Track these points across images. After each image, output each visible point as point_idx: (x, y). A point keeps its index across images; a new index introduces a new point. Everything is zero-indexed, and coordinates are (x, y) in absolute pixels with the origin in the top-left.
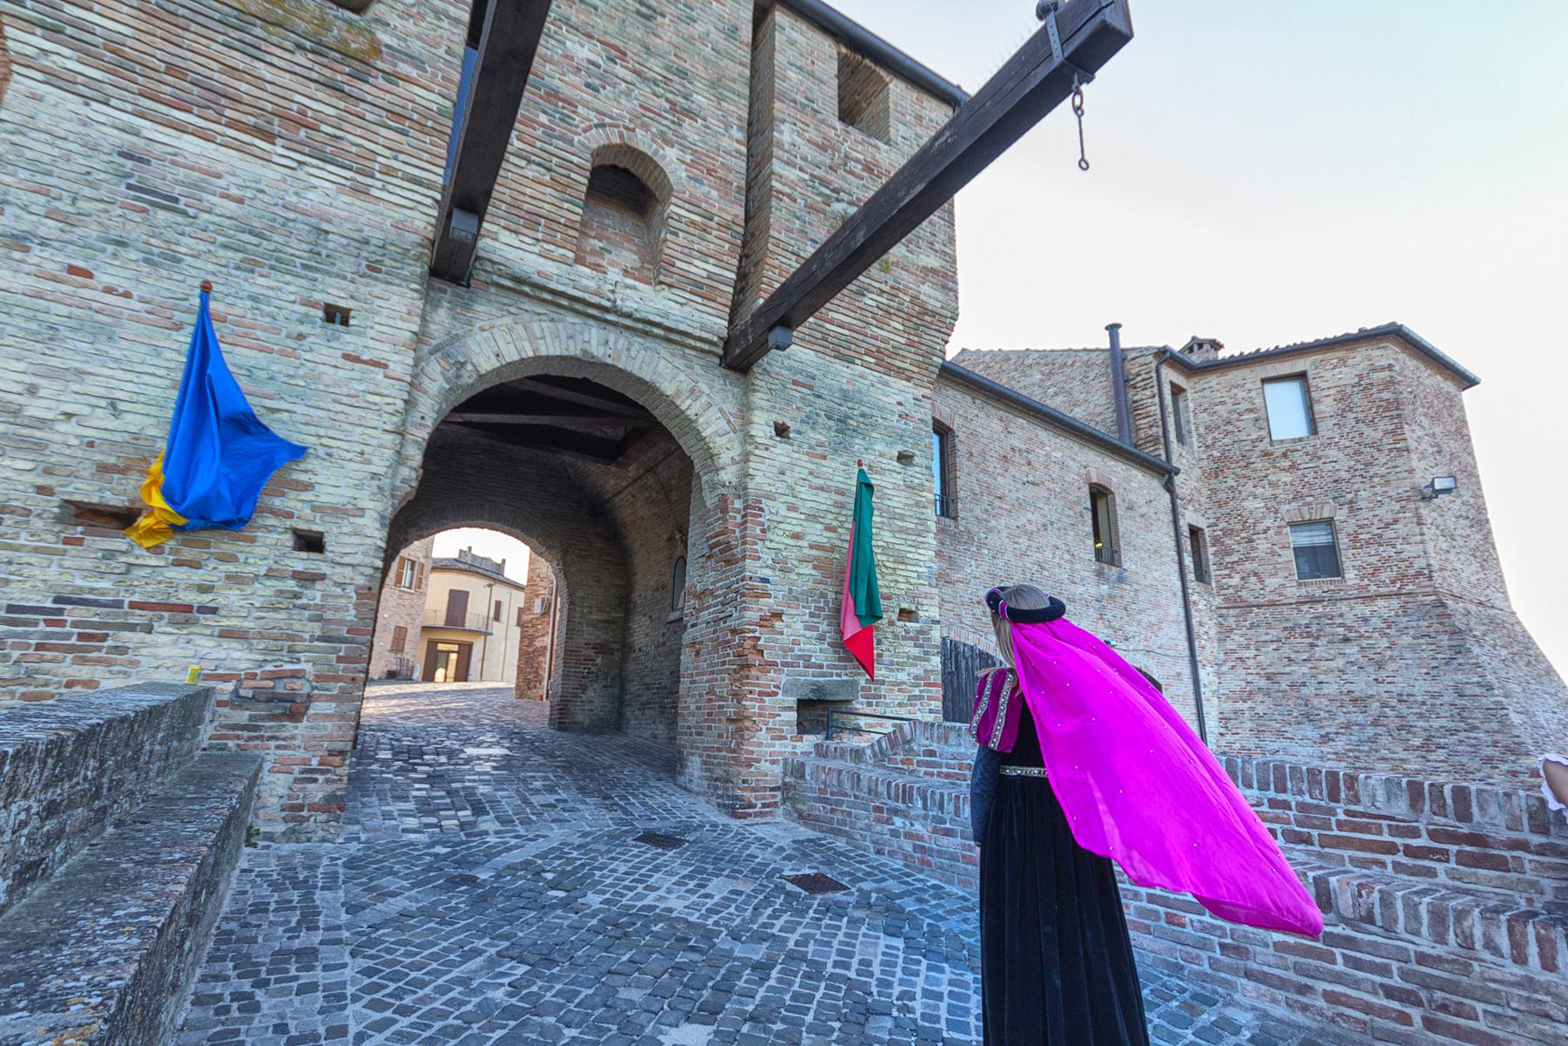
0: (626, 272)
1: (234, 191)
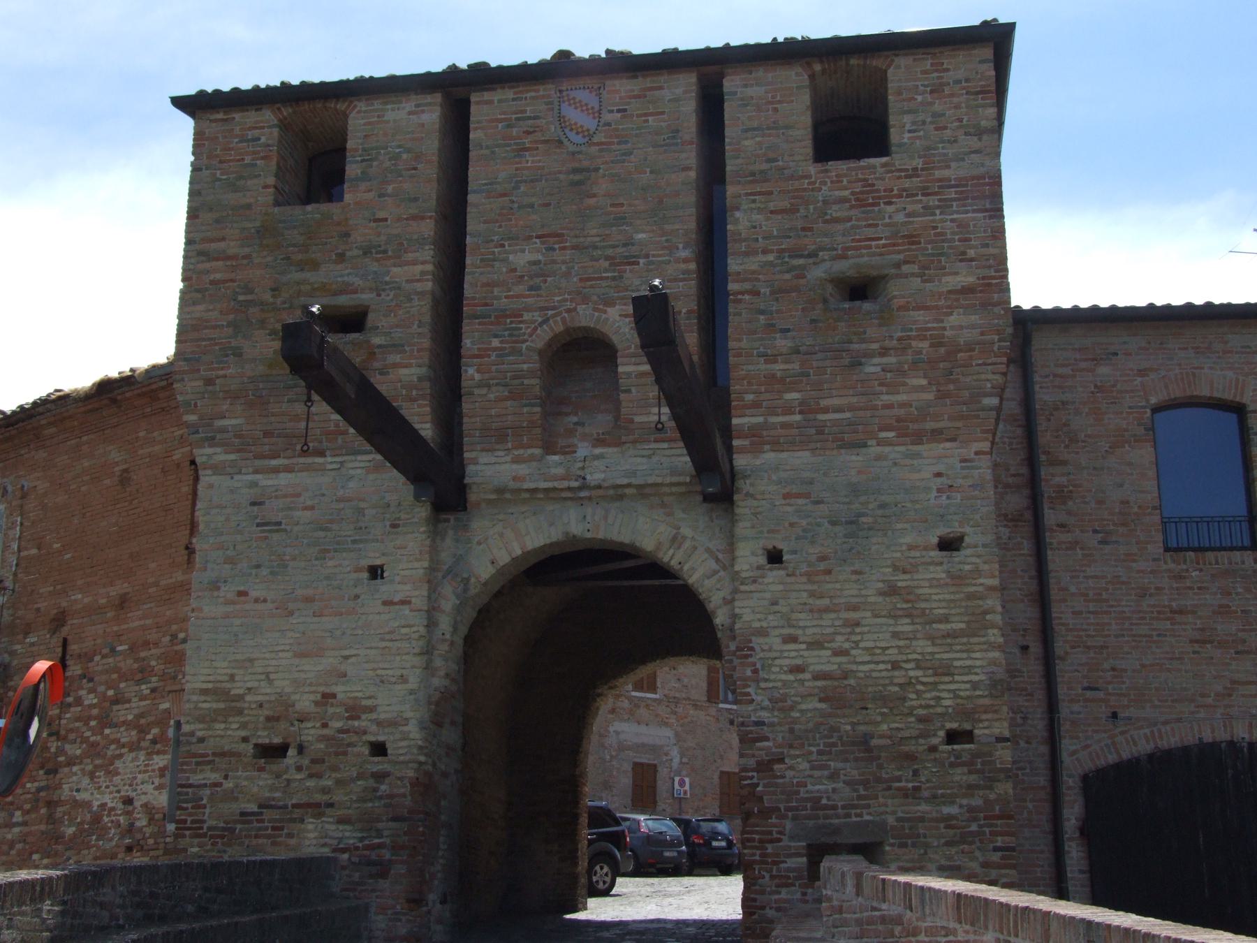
1: (309, 503)
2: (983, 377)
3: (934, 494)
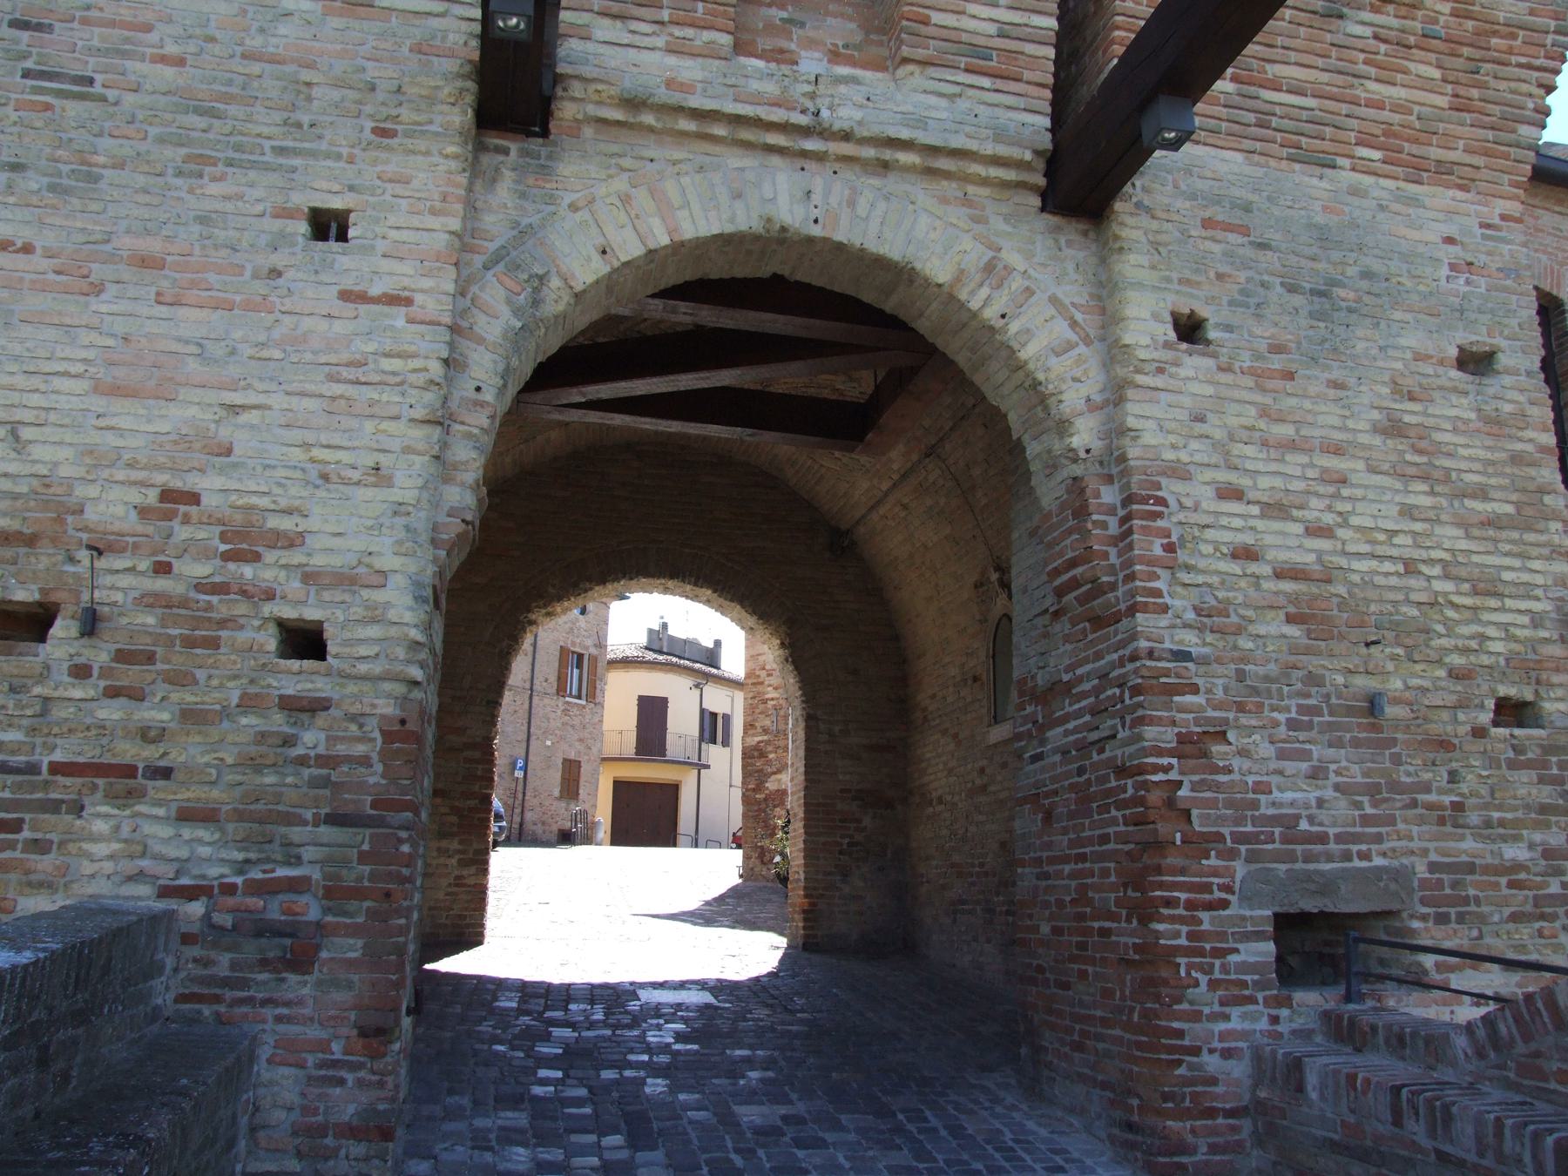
0: (835, 56)
1: (171, 49)
2: (1524, 87)
3: (1445, 271)
